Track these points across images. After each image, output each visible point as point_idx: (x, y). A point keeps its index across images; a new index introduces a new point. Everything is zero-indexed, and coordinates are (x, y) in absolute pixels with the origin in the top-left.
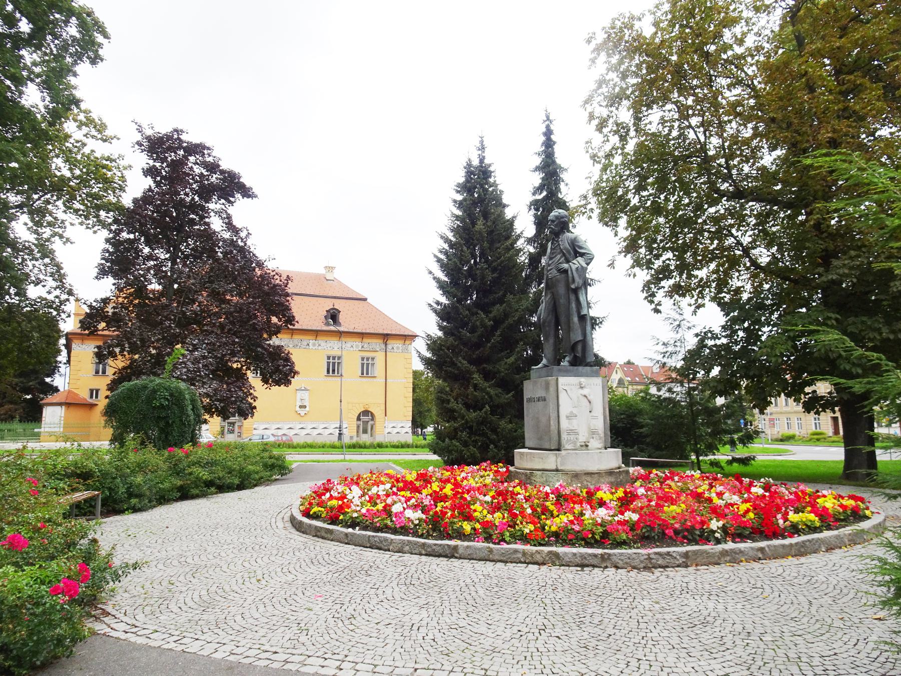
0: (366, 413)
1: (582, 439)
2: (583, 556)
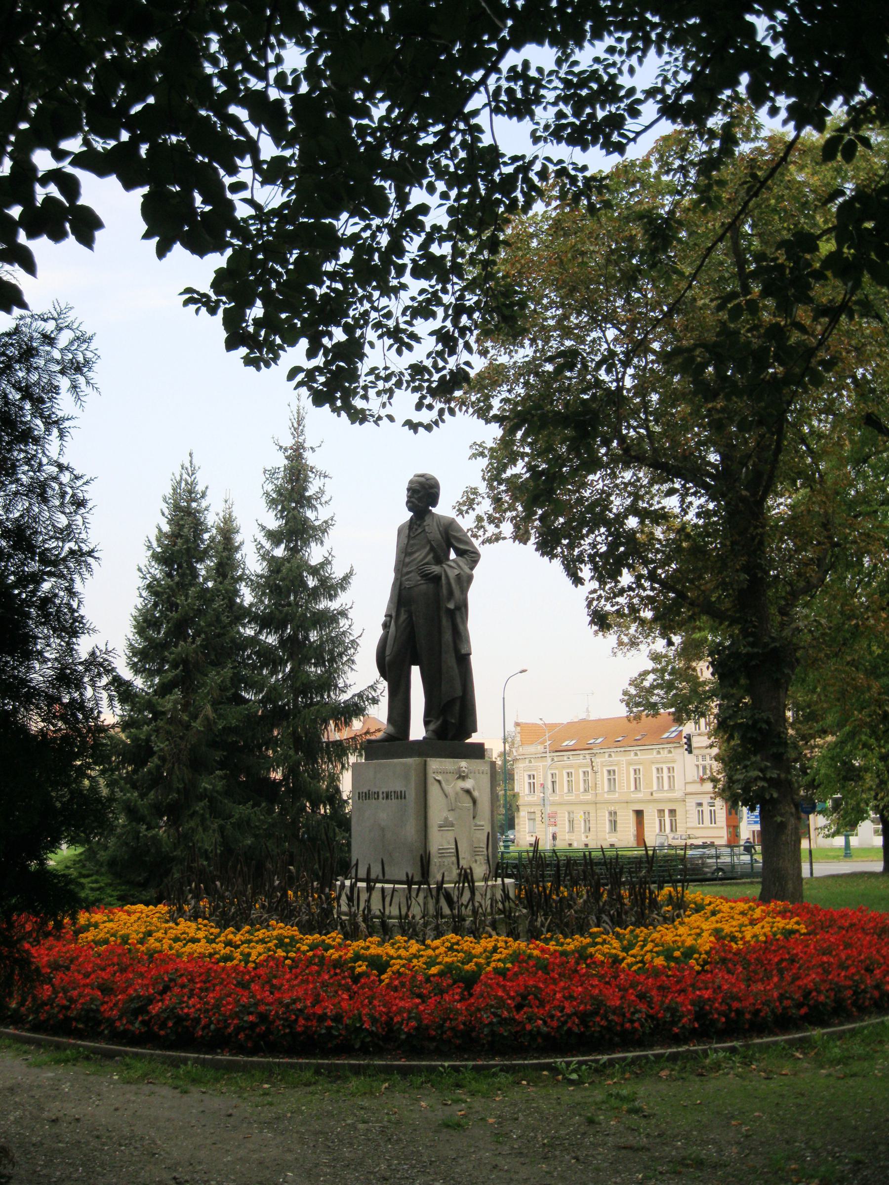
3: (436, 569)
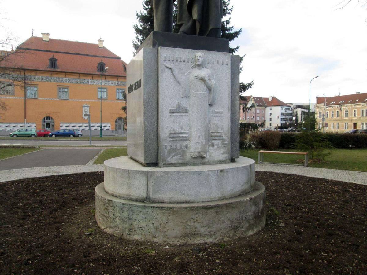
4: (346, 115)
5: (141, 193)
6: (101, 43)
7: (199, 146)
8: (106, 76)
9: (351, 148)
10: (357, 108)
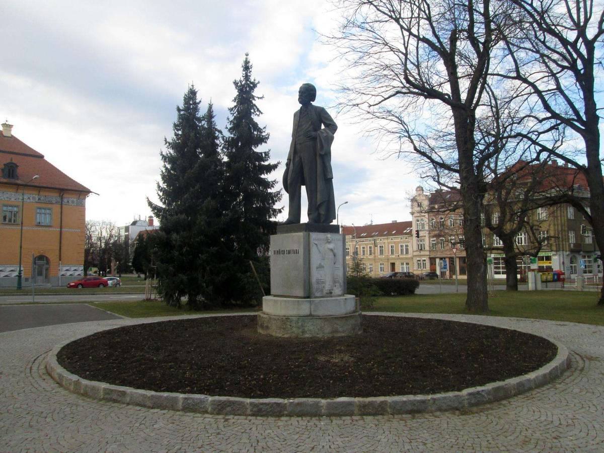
0: (41, 257)
1: (327, 287)
2: (413, 403)
3: (313, 133)
4: (381, 252)
5: (307, 312)
6: (8, 129)
7: (330, 286)
8: (18, 187)
9: (393, 295)
10: (395, 243)
